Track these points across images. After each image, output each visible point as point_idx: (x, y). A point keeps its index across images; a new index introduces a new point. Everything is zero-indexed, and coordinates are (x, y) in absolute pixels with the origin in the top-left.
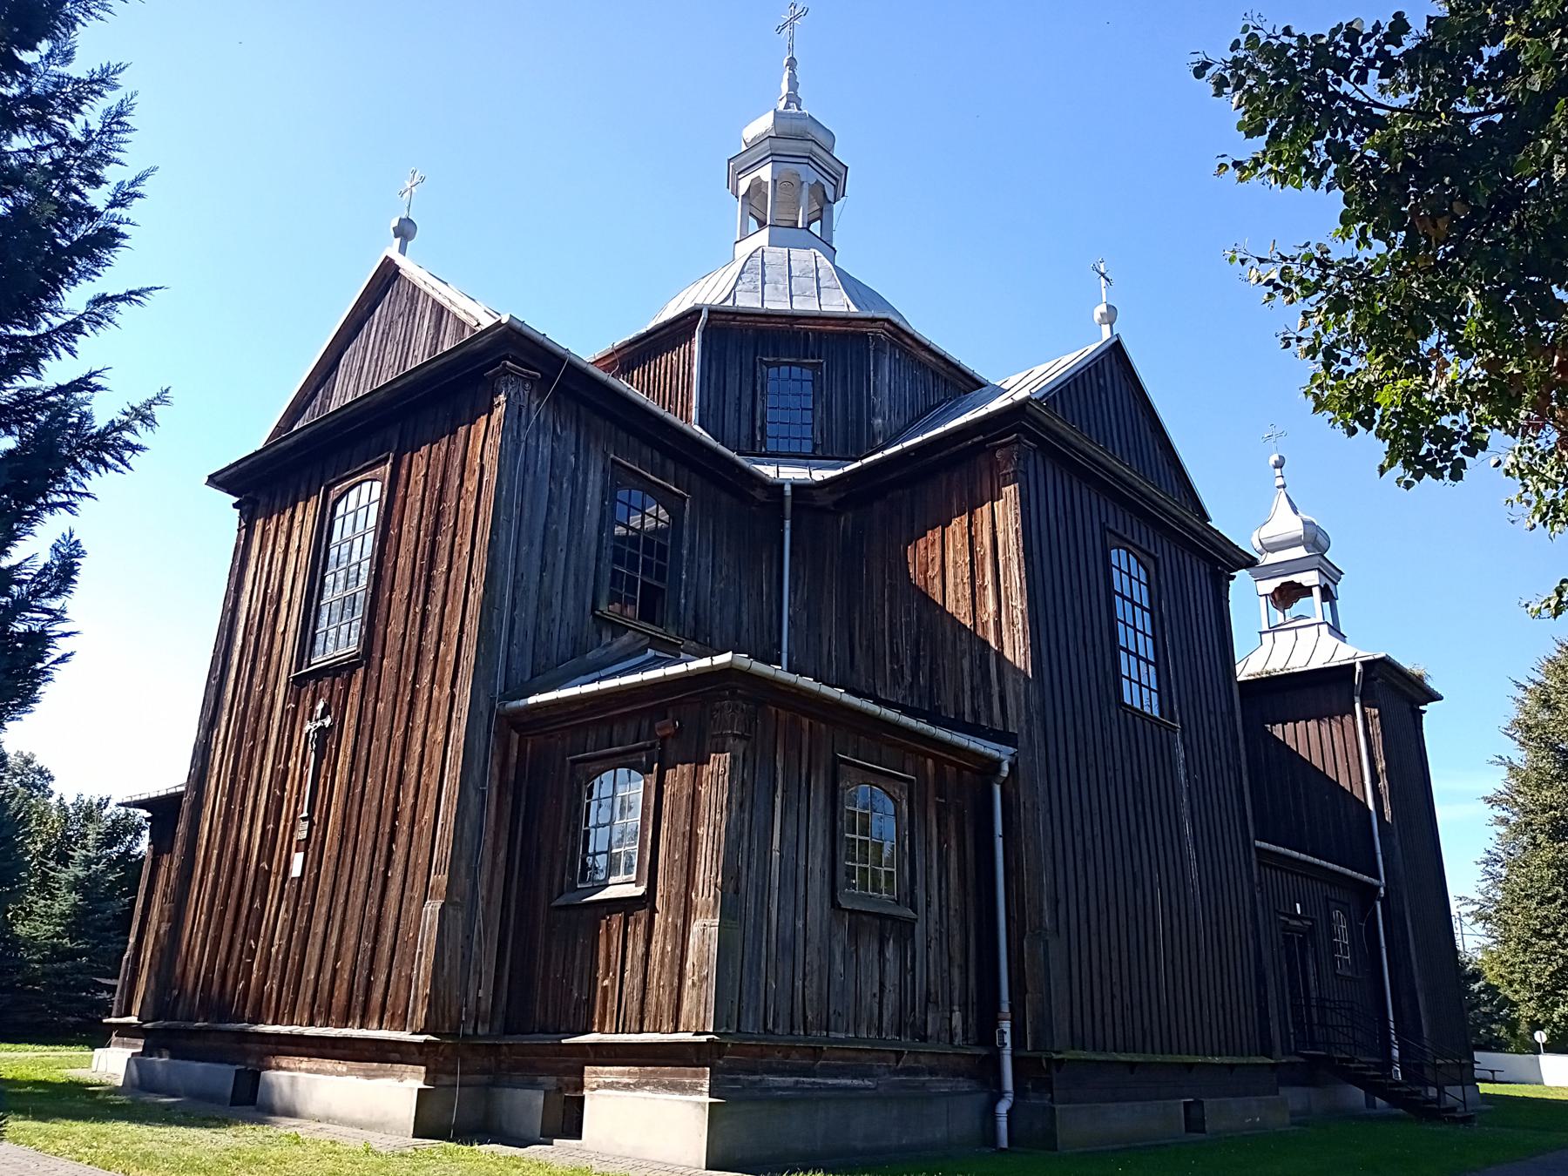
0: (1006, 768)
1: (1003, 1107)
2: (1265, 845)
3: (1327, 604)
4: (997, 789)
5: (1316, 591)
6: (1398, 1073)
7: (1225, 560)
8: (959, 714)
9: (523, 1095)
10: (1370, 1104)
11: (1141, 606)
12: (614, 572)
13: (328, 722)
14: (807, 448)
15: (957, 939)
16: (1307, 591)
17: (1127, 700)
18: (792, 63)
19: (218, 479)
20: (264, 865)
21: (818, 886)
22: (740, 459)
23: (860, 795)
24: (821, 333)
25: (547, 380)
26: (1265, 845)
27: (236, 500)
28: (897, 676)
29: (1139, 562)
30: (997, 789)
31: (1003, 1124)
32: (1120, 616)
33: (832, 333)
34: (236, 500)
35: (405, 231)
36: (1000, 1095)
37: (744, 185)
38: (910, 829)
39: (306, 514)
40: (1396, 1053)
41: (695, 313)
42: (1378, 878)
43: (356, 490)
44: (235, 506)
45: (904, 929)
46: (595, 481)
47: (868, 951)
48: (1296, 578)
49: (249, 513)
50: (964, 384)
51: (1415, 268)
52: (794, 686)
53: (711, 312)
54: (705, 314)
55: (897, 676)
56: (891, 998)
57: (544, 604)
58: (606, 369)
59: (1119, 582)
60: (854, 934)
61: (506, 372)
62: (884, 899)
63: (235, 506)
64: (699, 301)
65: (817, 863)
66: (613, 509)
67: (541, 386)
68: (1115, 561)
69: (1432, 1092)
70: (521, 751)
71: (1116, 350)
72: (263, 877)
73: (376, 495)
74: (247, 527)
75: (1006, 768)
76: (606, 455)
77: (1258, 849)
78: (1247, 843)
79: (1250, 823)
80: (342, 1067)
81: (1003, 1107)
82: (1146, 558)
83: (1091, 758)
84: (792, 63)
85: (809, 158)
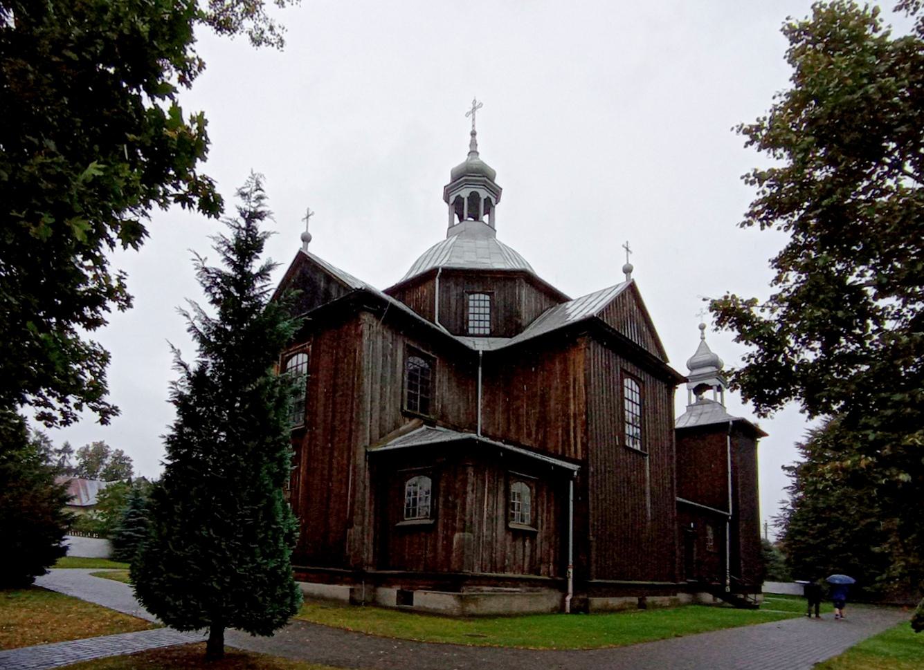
1: (568, 598)
2: (681, 500)
3: (719, 394)
5: (715, 388)
6: (728, 589)
7: (673, 379)
8: (557, 451)
9: (388, 590)
10: (714, 600)
11: (629, 400)
12: (409, 393)
14: (488, 331)
16: (711, 388)
17: (627, 444)
18: (473, 134)
21: (501, 522)
22: (457, 338)
23: (517, 487)
26: (681, 500)
28: (529, 435)
29: (636, 384)
31: (568, 604)
32: (626, 408)
35: (306, 239)
36: (567, 594)
37: (452, 199)
38: (536, 499)
40: (728, 581)
42: (728, 512)
43: (295, 357)
45: (532, 536)
46: (400, 353)
48: (706, 382)
50: (556, 298)
51: (783, 122)
52: (495, 446)
53: (443, 269)
54: (440, 271)
55: (529, 435)
56: (527, 560)
57: (383, 409)
59: (627, 393)
60: (514, 539)
62: (525, 526)
64: (436, 265)
65: (501, 512)
67: (377, 315)
68: (626, 384)
69: (742, 596)
71: (632, 288)
76: (404, 343)
77: (678, 502)
78: (673, 499)
80: (863, 605)
81: (568, 598)
84: (473, 134)
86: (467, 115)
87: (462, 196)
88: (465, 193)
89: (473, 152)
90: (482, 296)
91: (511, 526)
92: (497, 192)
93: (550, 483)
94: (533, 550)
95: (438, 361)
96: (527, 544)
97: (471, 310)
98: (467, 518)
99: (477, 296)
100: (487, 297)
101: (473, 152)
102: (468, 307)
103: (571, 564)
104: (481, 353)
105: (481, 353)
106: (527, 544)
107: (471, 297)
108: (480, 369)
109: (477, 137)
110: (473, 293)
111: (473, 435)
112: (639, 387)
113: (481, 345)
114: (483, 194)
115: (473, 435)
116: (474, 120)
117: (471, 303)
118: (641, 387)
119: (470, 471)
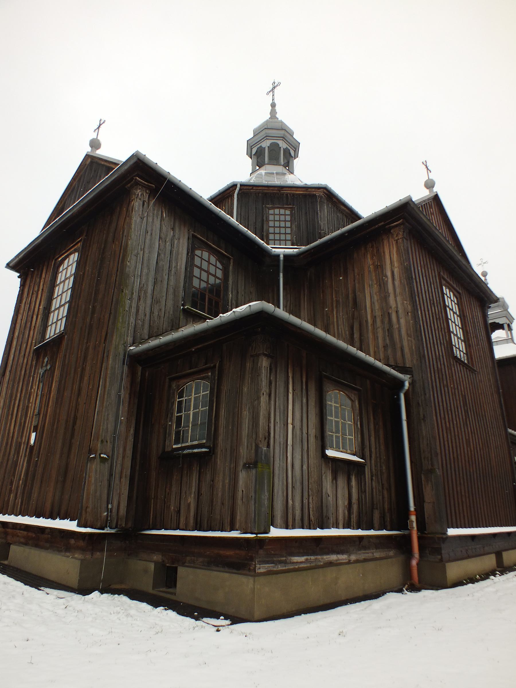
0: (407, 384)
1: (414, 563)
4: (402, 396)
13: (48, 367)
15: (385, 476)
19: (11, 265)
20: (19, 440)
24: (293, 195)
25: (156, 190)
27: (18, 274)
30: (402, 396)
33: (299, 195)
34: (18, 274)
37: (254, 151)
39: (46, 276)
41: (234, 186)
44: (19, 277)
47: (341, 482)
49: (24, 278)
53: (241, 185)
54: (239, 186)
57: (155, 301)
58: (205, 308)
61: (137, 183)
63: (19, 277)
66: (193, 259)
67: (152, 193)
70: (143, 374)
72: (19, 445)
73: (76, 259)
74: (23, 286)
75: (407, 384)
79: (506, 423)
81: (414, 563)
82: (458, 295)
83: (445, 382)
85: (283, 138)
86: (268, 94)
87: (263, 146)
88: (266, 144)
89: (273, 113)
90: (282, 211)
91: (330, 453)
92: (296, 146)
93: (377, 395)
94: (361, 491)
95: (232, 261)
96: (354, 483)
97: (271, 224)
98: (179, 267)
99: (277, 211)
100: (288, 212)
101: (273, 113)
102: (268, 221)
103: (412, 508)
104: (282, 257)
105: (282, 257)
106: (354, 483)
107: (271, 212)
108: (281, 275)
109: (277, 108)
110: (273, 208)
111: (269, 307)
112: (457, 298)
113: (281, 250)
114: (283, 145)
115: (269, 307)
116: (273, 95)
117: (271, 218)
118: (459, 298)
119: (264, 363)
